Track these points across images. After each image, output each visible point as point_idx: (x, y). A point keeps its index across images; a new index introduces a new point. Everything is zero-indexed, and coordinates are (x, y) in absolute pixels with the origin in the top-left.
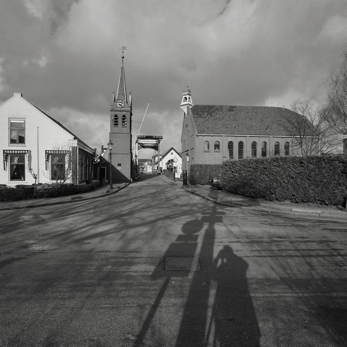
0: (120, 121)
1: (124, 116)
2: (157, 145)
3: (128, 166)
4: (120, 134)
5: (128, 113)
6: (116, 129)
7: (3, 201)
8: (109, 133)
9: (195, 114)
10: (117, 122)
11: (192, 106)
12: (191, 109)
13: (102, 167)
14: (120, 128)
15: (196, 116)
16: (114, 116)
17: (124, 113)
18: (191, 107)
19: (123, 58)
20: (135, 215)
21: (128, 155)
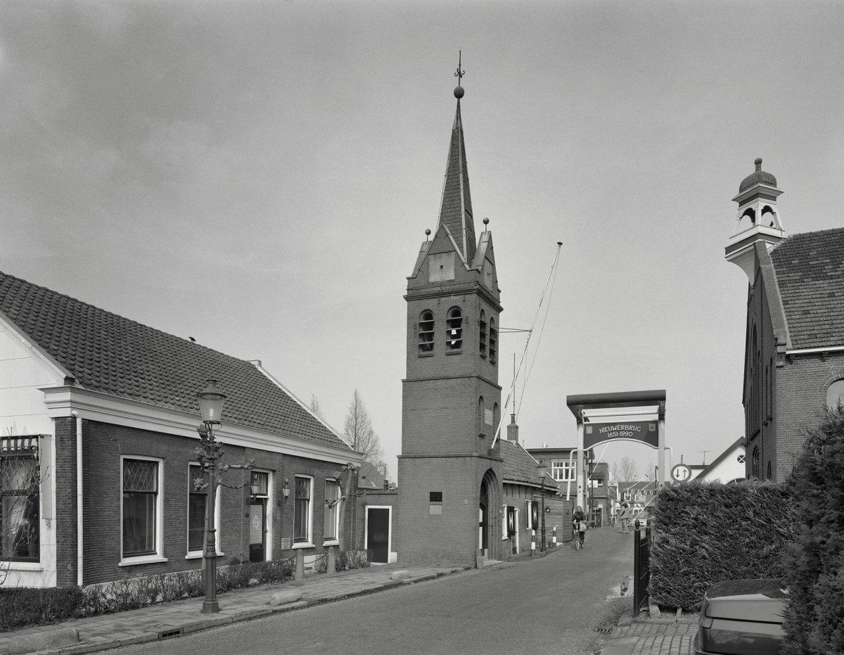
0: (440, 330)
1: (456, 312)
2: (654, 425)
3: (466, 501)
4: (439, 383)
5: (467, 297)
6: (428, 366)
7: (5, 630)
8: (403, 381)
9: (792, 269)
10: (430, 336)
11: (779, 244)
12: (775, 252)
13: (366, 547)
14: (441, 360)
15: (796, 276)
16: (418, 315)
17: (455, 300)
18: (770, 247)
19: (459, 94)
20: (357, 418)
21: (468, 459)
